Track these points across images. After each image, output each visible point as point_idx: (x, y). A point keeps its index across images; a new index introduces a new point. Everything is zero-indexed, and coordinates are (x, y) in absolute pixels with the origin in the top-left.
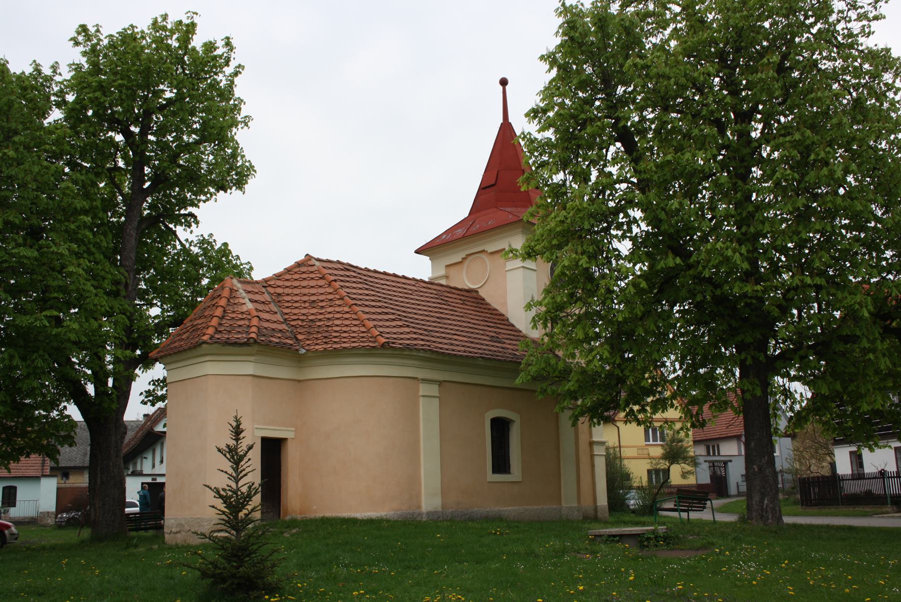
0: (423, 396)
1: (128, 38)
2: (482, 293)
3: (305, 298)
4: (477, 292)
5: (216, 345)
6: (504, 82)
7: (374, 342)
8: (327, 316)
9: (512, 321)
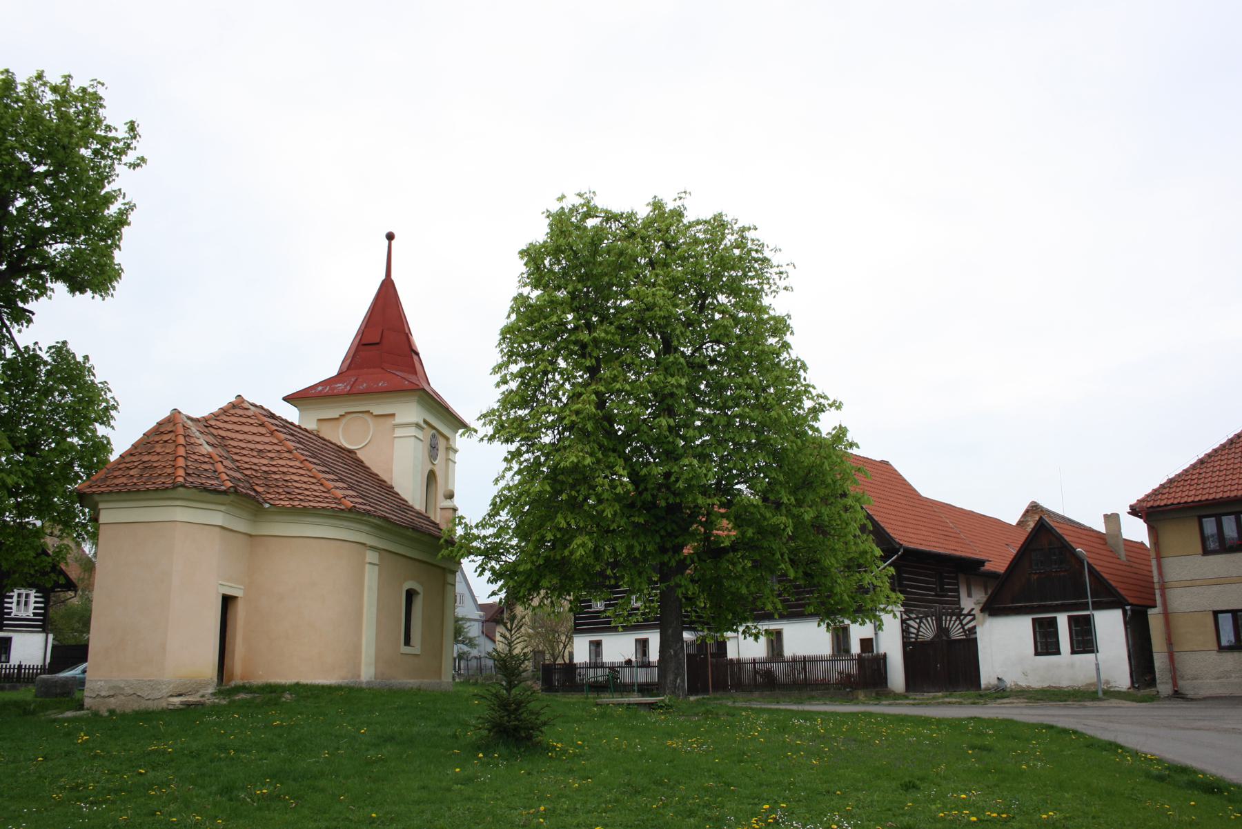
1: (798, 367)
2: (360, 455)
3: (253, 446)
6: (390, 237)
9: (396, 489)
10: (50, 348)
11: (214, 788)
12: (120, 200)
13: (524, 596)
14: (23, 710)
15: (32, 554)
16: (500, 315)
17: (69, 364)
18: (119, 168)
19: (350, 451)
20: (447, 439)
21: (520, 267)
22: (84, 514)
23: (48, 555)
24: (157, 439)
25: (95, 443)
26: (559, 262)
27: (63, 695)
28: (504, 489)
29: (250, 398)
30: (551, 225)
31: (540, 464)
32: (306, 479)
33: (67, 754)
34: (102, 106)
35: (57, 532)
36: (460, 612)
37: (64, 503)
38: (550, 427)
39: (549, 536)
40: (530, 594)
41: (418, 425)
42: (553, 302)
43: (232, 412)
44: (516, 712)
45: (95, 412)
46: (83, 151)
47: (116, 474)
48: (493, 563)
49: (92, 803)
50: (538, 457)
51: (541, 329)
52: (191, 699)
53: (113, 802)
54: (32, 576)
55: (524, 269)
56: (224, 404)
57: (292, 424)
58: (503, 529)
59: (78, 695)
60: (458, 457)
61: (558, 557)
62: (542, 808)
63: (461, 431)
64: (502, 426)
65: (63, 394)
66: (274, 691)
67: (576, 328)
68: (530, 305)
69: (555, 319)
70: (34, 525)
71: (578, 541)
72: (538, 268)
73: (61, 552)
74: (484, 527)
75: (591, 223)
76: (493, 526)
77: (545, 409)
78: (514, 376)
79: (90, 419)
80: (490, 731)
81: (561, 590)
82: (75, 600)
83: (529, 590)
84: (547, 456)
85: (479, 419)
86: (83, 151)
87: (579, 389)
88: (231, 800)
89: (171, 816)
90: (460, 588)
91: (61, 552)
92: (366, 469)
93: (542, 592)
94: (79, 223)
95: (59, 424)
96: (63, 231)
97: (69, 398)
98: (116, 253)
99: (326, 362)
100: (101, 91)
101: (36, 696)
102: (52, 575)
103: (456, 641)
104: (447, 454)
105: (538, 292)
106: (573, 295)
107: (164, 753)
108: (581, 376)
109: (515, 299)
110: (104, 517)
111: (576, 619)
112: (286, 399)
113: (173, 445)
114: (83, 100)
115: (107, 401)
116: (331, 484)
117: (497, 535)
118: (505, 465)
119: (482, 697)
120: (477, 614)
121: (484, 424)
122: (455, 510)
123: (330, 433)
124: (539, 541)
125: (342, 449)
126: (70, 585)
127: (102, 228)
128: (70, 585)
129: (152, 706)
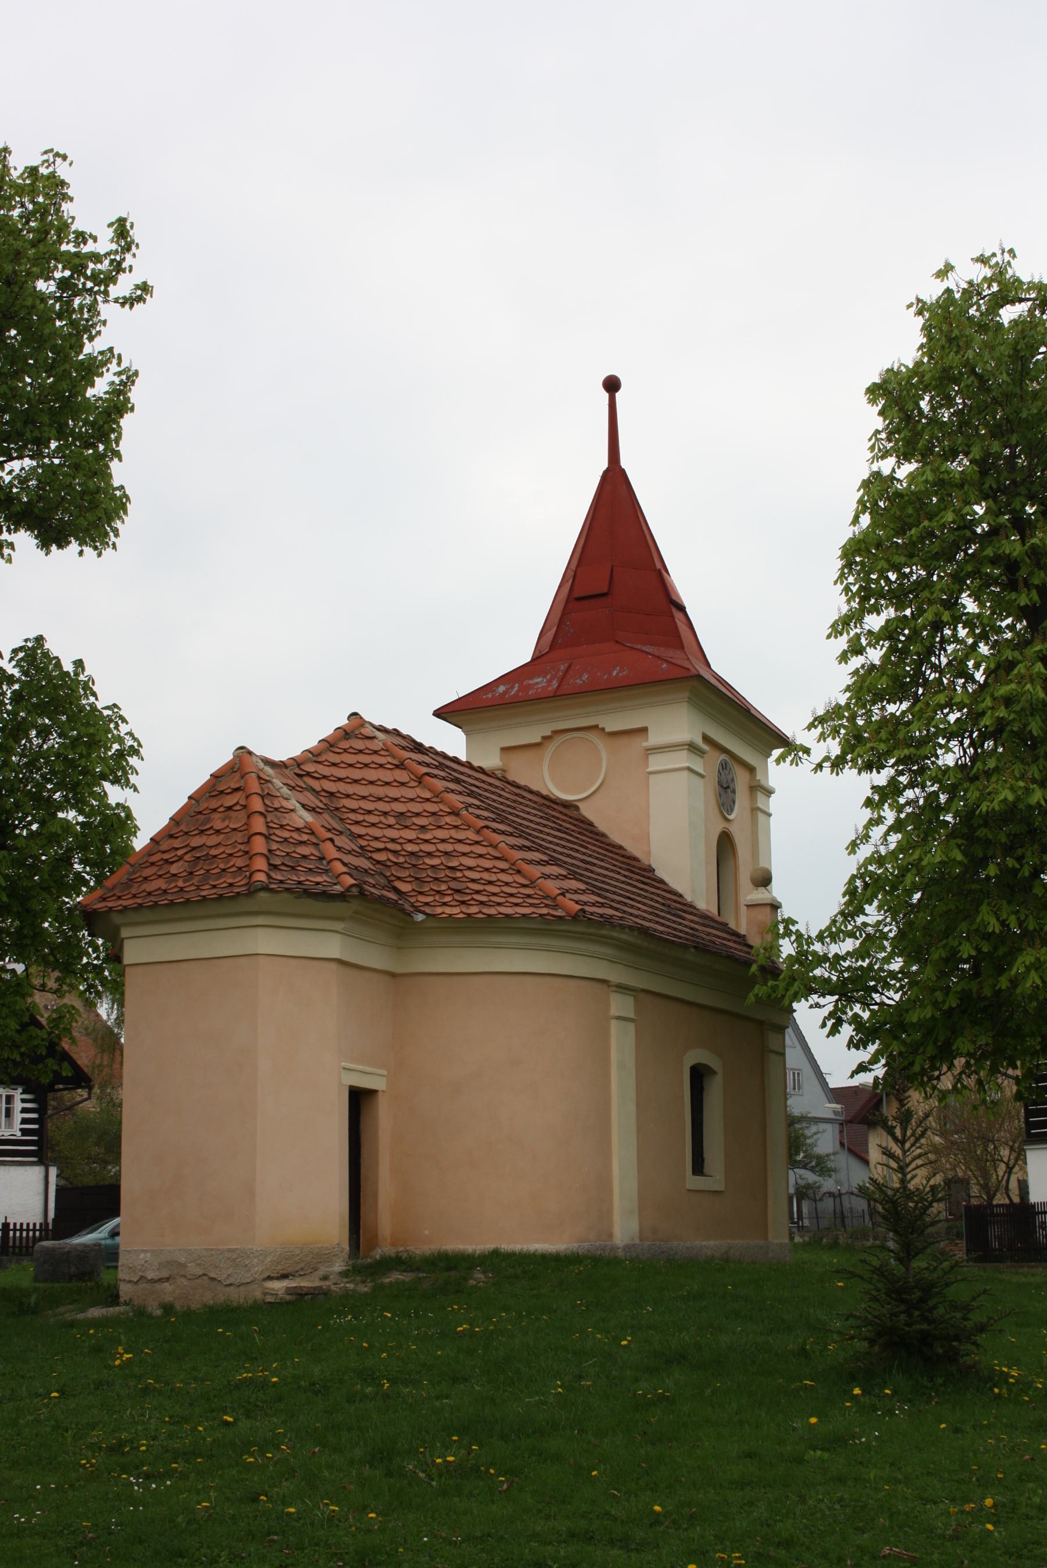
0: (619, 1018)
2: (587, 811)
3: (386, 807)
4: (577, 808)
5: (286, 895)
6: (612, 385)
7: (556, 907)
8: (442, 847)
9: (660, 873)
10: (15, 651)
11: (358, 1453)
12: (113, 367)
13: (923, 1072)
14: (19, 1305)
15: (14, 1025)
16: (836, 516)
17: (50, 679)
18: (106, 310)
19: (567, 805)
20: (751, 770)
21: (871, 419)
22: (96, 949)
23: (40, 1026)
24: (214, 804)
25: (105, 818)
26: (949, 402)
27: (81, 1276)
28: (869, 861)
29: (374, 716)
30: (926, 329)
31: (940, 809)
32: (488, 864)
33: (99, 1385)
34: (66, 197)
35: (52, 984)
36: (797, 1105)
37: (60, 931)
38: (955, 733)
39: (967, 950)
40: (934, 1068)
41: (692, 747)
42: (943, 484)
43: (345, 744)
44: (915, 1303)
45: (104, 760)
46: (41, 285)
47: (147, 872)
48: (857, 1008)
49: (147, 1476)
50: (935, 794)
51: (922, 539)
52: (305, 1283)
53: (183, 1476)
54: (16, 1064)
55: (879, 423)
56: (327, 731)
57: (455, 760)
58: (871, 941)
59: (106, 1277)
60: (774, 804)
61: (987, 992)
62: (989, 1502)
63: (777, 753)
64: (858, 738)
65: (44, 733)
66: (452, 1267)
67: (995, 531)
68: (898, 494)
69: (949, 516)
70: (13, 971)
71: (1026, 958)
72: (908, 418)
73: (61, 1018)
74: (834, 937)
75: (1008, 314)
76: (852, 935)
77: (942, 698)
78: (875, 638)
79: (93, 775)
80: (872, 1342)
81: (997, 1057)
82: (89, 1105)
83: (932, 1059)
84: (953, 792)
85: (811, 726)
86: (41, 285)
87: (1009, 654)
88: (389, 1474)
89: (285, 1504)
90: (793, 1057)
91: (61, 1018)
92: (599, 837)
93: (959, 1062)
94: (46, 419)
95: (41, 787)
96: (20, 435)
97: (54, 741)
98: (114, 465)
99: (510, 640)
100: (63, 171)
101: (36, 1279)
102: (50, 1061)
103: (793, 1164)
104: (753, 798)
105: (908, 468)
106: (984, 465)
107: (264, 1384)
108: (1011, 627)
109: (866, 484)
110: (131, 953)
111: (1029, 1114)
112: (439, 713)
113: (243, 814)
114: (33, 192)
115: (120, 740)
116: (536, 871)
117: (859, 954)
118: (867, 814)
119: (853, 1275)
120: (829, 1109)
121: (822, 737)
122: (775, 906)
123: (523, 773)
124: (946, 961)
125: (550, 801)
126: (80, 1079)
127: (86, 422)
128: (80, 1079)
129: (236, 1296)
